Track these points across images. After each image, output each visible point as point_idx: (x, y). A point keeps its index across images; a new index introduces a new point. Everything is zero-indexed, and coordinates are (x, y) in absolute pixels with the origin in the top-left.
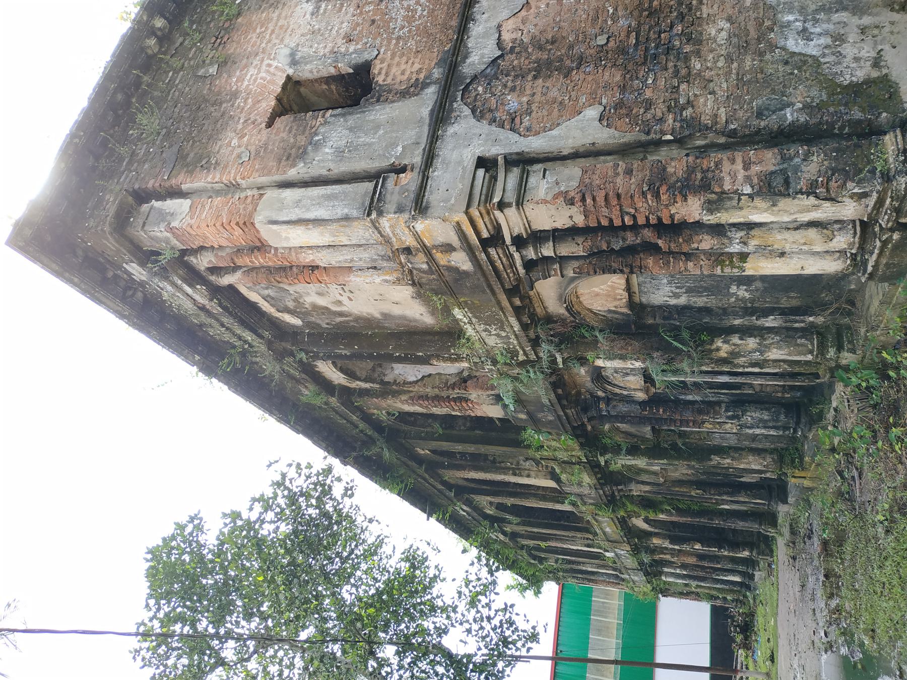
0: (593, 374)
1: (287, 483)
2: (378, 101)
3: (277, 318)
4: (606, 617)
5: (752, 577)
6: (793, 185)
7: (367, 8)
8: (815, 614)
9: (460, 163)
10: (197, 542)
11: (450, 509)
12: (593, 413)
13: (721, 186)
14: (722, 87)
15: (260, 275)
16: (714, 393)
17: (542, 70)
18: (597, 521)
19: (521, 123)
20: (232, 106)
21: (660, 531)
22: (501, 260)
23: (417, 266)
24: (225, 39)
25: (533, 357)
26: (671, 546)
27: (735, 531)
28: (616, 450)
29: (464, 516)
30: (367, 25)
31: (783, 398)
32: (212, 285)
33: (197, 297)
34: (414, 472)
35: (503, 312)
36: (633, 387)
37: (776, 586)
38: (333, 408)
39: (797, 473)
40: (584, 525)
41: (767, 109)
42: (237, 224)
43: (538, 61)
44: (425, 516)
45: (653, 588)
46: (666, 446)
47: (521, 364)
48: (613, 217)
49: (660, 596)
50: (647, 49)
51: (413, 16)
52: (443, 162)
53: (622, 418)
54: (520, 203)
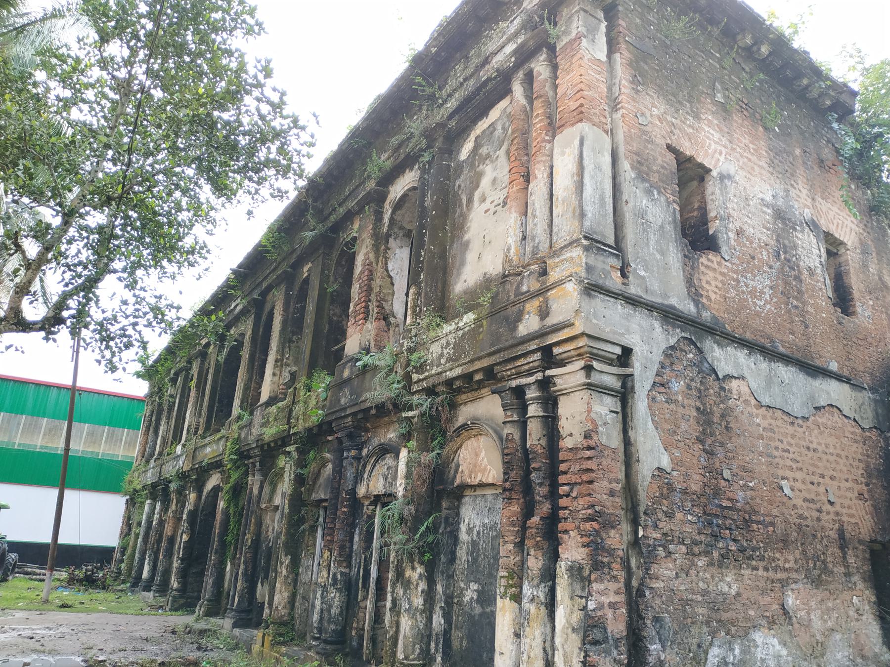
0: (390, 445)
1: (295, 131)
2: (685, 256)
3: (469, 135)
4: (106, 441)
5: (147, 588)
6: (594, 648)
7: (764, 253)
8: (121, 651)
9: (628, 331)
10: (235, 28)
11: (239, 293)
12: (346, 443)
13: (596, 581)
14: (681, 586)
15: (521, 123)
16: (360, 562)
17: (704, 415)
18: (219, 439)
19: (659, 393)
20: (687, 113)
21: (203, 501)
22: (527, 363)
23: (525, 281)
24: (745, 113)
25: (415, 388)
26: (186, 511)
27: (202, 574)
28: (301, 463)
29: (230, 306)
30: (751, 251)
31: (351, 628)
32: (513, 73)
33: (499, 57)
34: (284, 260)
35: (468, 362)
36: (371, 483)
37: (140, 613)
38: (363, 183)
39: (268, 639)
40: (213, 427)
41: (661, 627)
42: (582, 105)
43: (712, 413)
44: (235, 266)
45: (137, 491)
46: (302, 513)
47: (407, 377)
48: (568, 476)
49: (128, 497)
50: (717, 516)
51: (756, 297)
52: (629, 315)
53: (339, 471)
54: (590, 386)
